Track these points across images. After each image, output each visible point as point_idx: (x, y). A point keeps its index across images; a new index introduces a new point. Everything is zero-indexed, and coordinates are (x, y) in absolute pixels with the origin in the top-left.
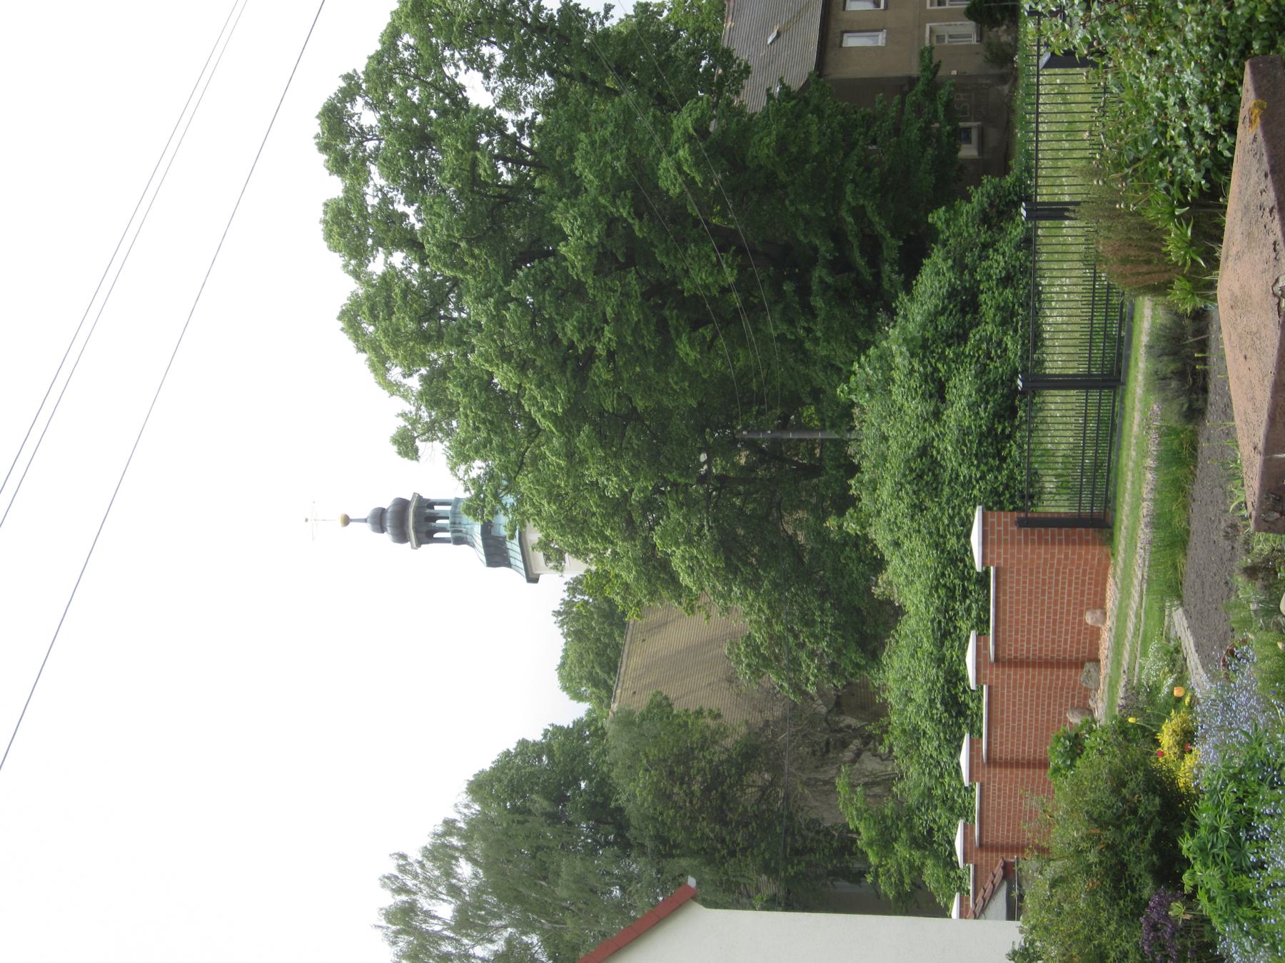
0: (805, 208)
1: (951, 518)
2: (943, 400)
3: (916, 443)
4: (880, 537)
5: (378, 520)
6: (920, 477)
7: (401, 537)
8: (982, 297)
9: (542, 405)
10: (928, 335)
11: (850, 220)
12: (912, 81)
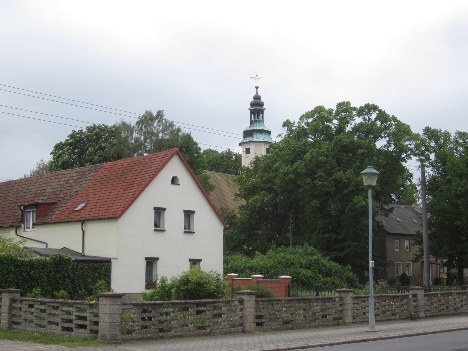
0: (351, 232)
1: (278, 271)
2: (305, 268)
3: (294, 262)
4: (270, 253)
5: (257, 98)
6: (287, 263)
7: (252, 105)
8: (329, 277)
9: (299, 165)
10: (320, 265)
11: (348, 244)
12: (385, 258)
